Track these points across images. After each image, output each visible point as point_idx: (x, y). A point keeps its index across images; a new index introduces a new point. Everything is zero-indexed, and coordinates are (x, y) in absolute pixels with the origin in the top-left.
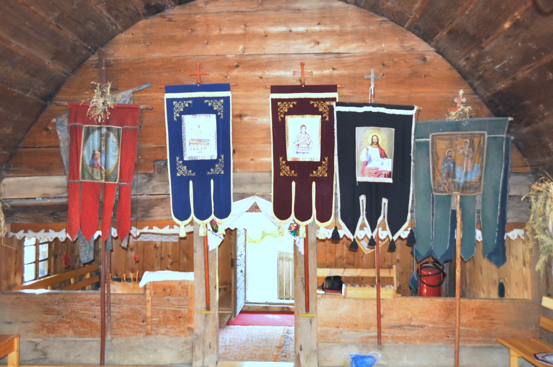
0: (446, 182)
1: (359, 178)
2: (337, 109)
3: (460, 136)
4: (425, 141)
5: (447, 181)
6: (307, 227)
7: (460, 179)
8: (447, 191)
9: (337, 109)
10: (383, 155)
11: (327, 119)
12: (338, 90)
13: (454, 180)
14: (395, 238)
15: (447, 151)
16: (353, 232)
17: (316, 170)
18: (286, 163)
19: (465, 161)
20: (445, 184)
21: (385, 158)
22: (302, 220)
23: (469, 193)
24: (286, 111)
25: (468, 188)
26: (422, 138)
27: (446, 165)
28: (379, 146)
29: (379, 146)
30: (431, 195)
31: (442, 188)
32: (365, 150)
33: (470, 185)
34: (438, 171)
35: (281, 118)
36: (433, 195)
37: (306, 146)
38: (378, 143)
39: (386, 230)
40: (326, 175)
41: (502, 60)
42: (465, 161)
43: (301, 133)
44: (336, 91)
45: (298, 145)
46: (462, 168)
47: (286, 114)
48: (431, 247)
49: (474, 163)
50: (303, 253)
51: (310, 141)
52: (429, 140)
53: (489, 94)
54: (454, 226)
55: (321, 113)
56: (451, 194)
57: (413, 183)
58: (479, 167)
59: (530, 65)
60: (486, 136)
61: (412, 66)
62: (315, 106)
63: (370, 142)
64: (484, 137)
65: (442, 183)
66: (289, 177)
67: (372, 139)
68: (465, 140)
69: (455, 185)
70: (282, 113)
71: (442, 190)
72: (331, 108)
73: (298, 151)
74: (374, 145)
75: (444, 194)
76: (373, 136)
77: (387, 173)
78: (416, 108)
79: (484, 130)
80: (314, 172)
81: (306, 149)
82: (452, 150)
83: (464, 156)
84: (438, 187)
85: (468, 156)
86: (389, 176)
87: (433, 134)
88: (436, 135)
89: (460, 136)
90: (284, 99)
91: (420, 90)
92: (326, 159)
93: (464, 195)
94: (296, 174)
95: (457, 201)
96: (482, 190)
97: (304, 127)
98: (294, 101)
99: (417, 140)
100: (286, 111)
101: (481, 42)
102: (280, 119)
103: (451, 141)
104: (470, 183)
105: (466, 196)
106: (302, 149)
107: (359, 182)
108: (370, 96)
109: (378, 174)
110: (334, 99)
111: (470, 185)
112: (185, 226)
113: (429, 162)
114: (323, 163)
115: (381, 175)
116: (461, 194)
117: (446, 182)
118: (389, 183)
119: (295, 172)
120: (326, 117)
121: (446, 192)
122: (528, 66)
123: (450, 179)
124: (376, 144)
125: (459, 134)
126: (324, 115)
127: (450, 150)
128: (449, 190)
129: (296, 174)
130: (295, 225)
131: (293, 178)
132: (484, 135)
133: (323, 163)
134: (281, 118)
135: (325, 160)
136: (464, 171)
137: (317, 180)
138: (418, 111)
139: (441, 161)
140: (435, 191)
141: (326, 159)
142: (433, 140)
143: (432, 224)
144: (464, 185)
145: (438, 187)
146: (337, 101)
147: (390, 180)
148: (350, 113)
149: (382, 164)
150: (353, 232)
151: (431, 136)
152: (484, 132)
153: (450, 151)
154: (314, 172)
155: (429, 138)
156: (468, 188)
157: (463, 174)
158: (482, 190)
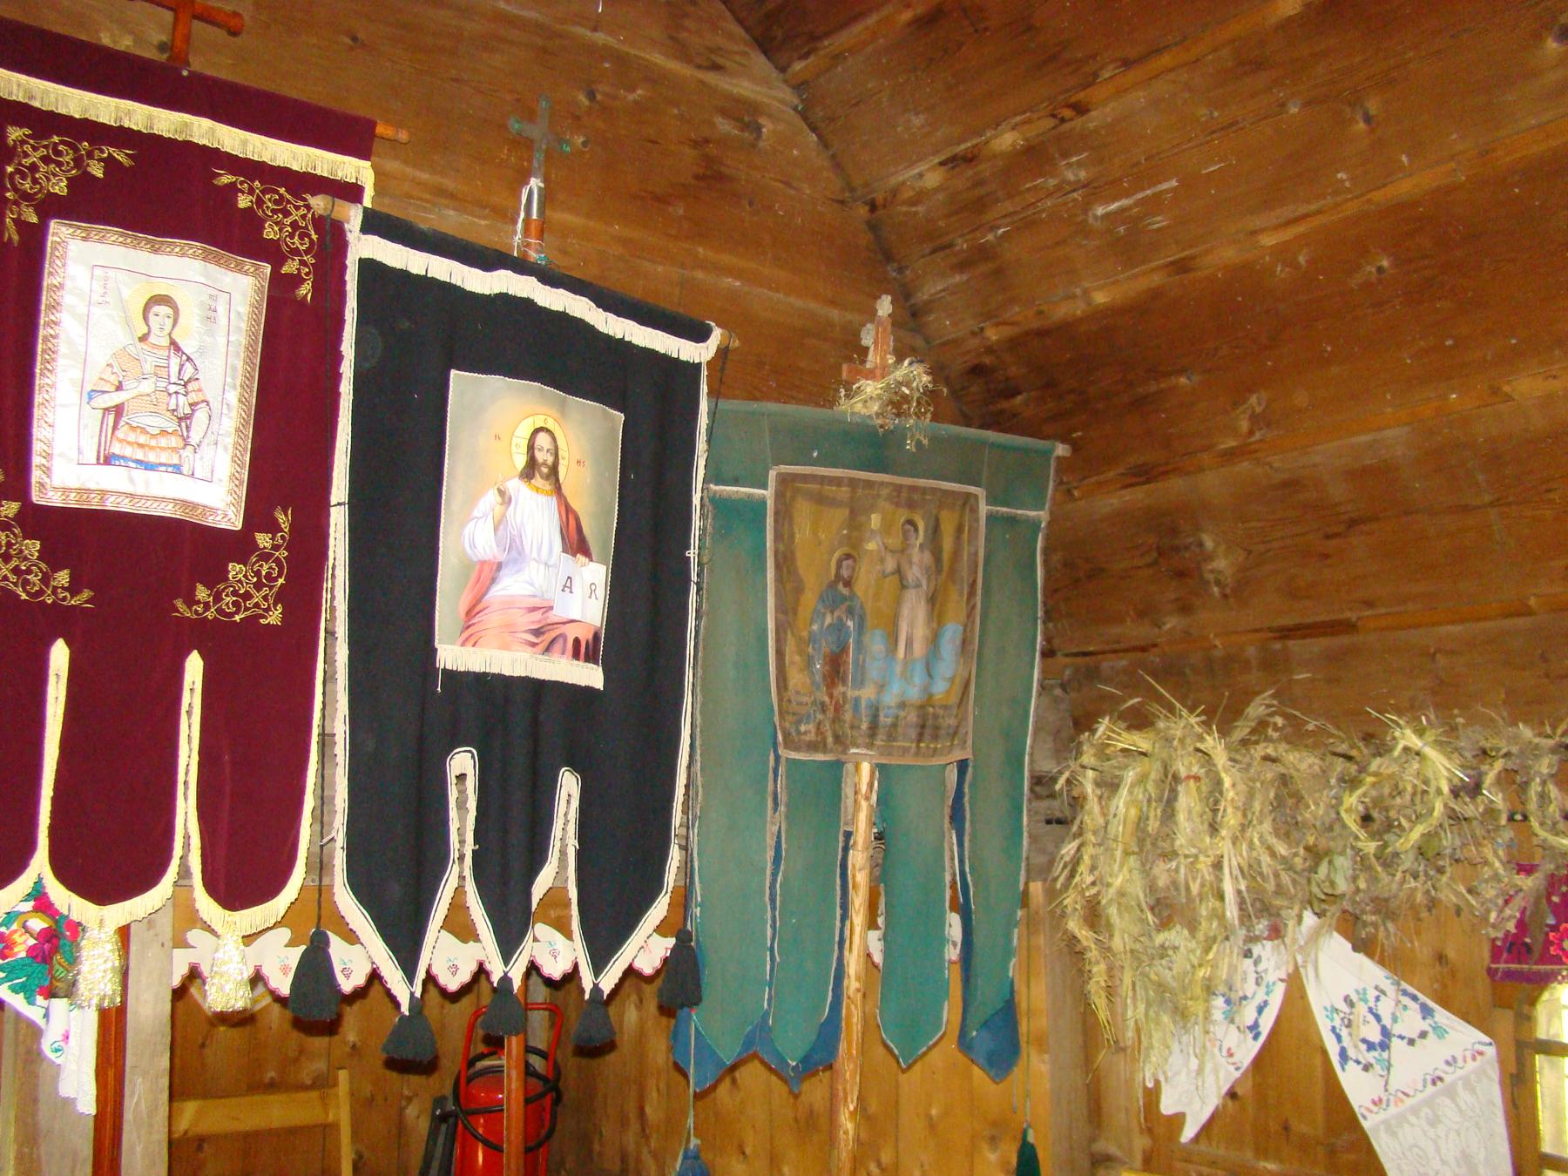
1: (451, 655)
2: (364, 247)
4: (750, 496)
5: (831, 696)
6: (124, 933)
7: (882, 687)
9: (364, 247)
10: (576, 544)
11: (305, 290)
12: (372, 158)
14: (608, 982)
15: (837, 555)
16: (406, 948)
17: (216, 578)
18: (20, 517)
20: (823, 708)
21: (581, 558)
22: (102, 891)
24: (60, 187)
26: (736, 482)
27: (828, 620)
28: (558, 489)
29: (558, 489)
32: (491, 497)
35: (20, 224)
37: (172, 426)
38: (554, 469)
39: (477, 939)
40: (274, 617)
41: (1144, 175)
43: (143, 339)
44: (362, 153)
45: (119, 410)
47: (52, 208)
48: (767, 1014)
50: (87, 1104)
51: (193, 397)
52: (768, 494)
53: (993, 335)
55: (272, 253)
59: (1303, 209)
60: (984, 508)
61: (707, 141)
62: (243, 202)
63: (521, 461)
64: (974, 510)
66: (35, 608)
67: (531, 447)
70: (26, 197)
72: (332, 239)
73: (116, 449)
74: (538, 481)
75: (820, 757)
76: (537, 431)
77: (585, 636)
78: (717, 336)
79: (977, 485)
80: (202, 593)
81: (163, 442)
86: (591, 657)
88: (796, 477)
89: (885, 492)
90: (51, 114)
91: (727, 259)
92: (283, 520)
93: (894, 761)
94: (87, 594)
97: (164, 310)
98: (119, 146)
100: (60, 187)
101: (1091, 81)
102: (12, 233)
103: (853, 513)
106: (142, 439)
107: (450, 675)
108: (520, 225)
109: (545, 636)
110: (352, 192)
112: (249, 939)
114: (263, 540)
115: (558, 646)
116: (884, 761)
117: (826, 699)
118: (589, 690)
119: (73, 578)
120: (297, 280)
121: (825, 750)
122: (1288, 211)
124: (547, 478)
125: (882, 484)
126: (290, 267)
128: (837, 738)
129: (87, 594)
130: (38, 924)
131: (60, 622)
132: (968, 501)
133: (263, 540)
134: (20, 224)
135: (273, 528)
137: (211, 637)
138: (723, 352)
139: (809, 599)
140: (789, 743)
141: (283, 520)
142: (779, 495)
143: (773, 900)
146: (367, 202)
147: (592, 676)
148: (426, 283)
149: (568, 585)
150: (406, 948)
151: (772, 474)
152: (972, 489)
154: (202, 593)
155: (764, 486)
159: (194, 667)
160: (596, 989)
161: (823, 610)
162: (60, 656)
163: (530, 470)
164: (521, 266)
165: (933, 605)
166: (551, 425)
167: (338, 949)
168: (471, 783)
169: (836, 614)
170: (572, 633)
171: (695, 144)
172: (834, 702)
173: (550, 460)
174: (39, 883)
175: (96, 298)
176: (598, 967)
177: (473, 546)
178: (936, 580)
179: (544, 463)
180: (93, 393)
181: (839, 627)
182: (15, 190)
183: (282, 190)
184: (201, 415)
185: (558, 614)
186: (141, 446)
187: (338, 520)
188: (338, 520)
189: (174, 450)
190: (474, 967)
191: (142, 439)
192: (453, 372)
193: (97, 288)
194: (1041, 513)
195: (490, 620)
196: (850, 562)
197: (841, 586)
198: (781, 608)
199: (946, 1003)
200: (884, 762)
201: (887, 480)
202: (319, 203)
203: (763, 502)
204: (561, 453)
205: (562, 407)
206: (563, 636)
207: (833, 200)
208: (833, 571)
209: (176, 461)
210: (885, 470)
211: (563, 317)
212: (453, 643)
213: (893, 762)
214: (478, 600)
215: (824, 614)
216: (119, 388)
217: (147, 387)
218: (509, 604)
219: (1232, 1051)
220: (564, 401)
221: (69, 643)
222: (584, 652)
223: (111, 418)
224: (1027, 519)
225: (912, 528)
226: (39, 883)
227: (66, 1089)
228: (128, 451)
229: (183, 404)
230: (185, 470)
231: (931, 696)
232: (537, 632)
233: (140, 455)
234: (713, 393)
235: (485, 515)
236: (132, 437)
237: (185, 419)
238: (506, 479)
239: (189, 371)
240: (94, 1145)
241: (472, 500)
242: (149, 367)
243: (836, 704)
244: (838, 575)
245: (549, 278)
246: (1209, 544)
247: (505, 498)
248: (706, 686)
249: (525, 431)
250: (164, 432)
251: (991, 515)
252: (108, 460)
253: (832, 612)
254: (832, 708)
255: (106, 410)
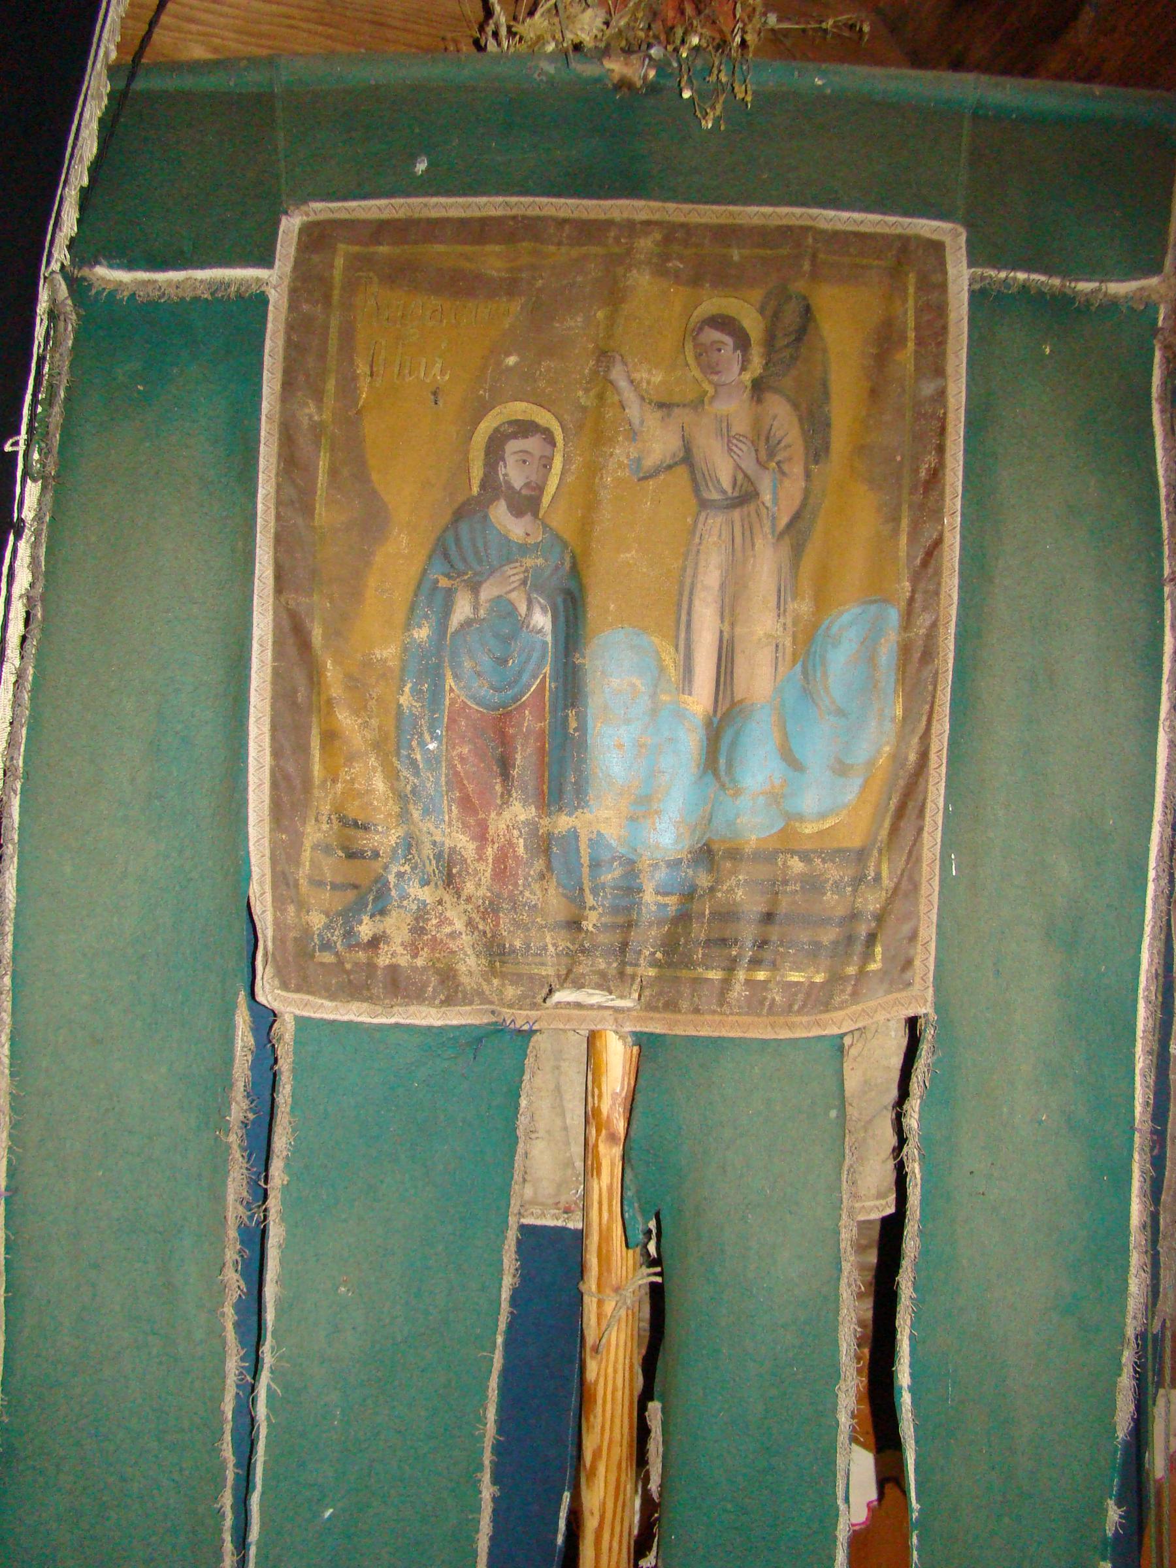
0: (465, 843)
3: (646, 244)
5: (482, 836)
8: (469, 964)
13: (564, 822)
19: (711, 576)
23: (757, 1002)
25: (748, 933)
30: (242, 1019)
31: (396, 926)
33: (774, 888)
34: (355, 684)
36: (265, 1020)
42: (711, 576)
46: (669, 657)
49: (822, 601)
54: (1153, 1224)
56: (521, 1018)
57: (1163, 411)
58: (887, 653)
65: (410, 844)
68: (713, 303)
69: (576, 899)
71: (394, 954)
82: (544, 418)
83: (704, 504)
84: (349, 916)
85: (745, 496)
87: (320, 210)
89: (646, 244)
93: (683, 1026)
95: (592, 1116)
96: (925, 960)
99: (106, 274)
104: (766, 856)
105: (717, 1043)
111: (774, 888)
113: (249, 558)
116: (656, 1027)
117: (465, 843)
123: (520, 811)
125: (632, 228)
127: (519, 409)
136: (700, 700)
144: (689, 895)
145: (349, 916)
151: (291, 225)
152: (926, 227)
153: (525, 428)
155: (266, 260)
156: (748, 933)
157: (690, 742)
158: (925, 960)
161: (444, 582)
165: (798, 551)
169: (487, 592)
172: (490, 852)
178: (808, 475)
194: (1154, 281)
197: (500, 513)
200: (657, 1028)
201: (643, 216)
203: (261, 301)
208: (477, 472)
210: (633, 188)
213: (679, 1031)
215: (449, 594)
225: (728, 340)
231: (793, 818)
240: (663, 1321)
243: (501, 859)
244: (491, 486)
251: (983, 292)
253: (475, 588)
254: (486, 871)
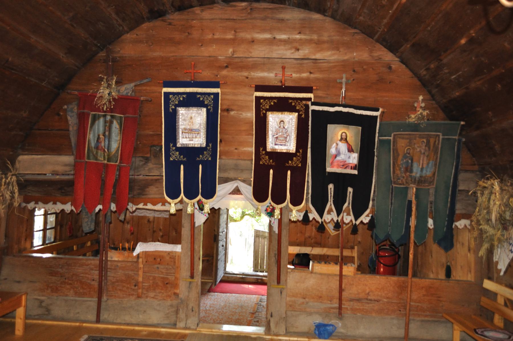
1: (329, 169)
4: (388, 139)
5: (405, 175)
6: (281, 209)
7: (416, 173)
10: (350, 150)
11: (303, 116)
12: (314, 92)
14: (358, 222)
15: (406, 148)
17: (292, 160)
20: (404, 177)
22: (278, 204)
24: (268, 107)
26: (385, 136)
27: (404, 161)
35: (263, 113)
39: (350, 215)
43: (280, 127)
45: (277, 138)
50: (277, 232)
51: (287, 134)
52: (391, 138)
53: (445, 101)
60: (441, 137)
62: (293, 104)
64: (439, 137)
67: (341, 136)
72: (307, 107)
73: (277, 143)
74: (343, 141)
75: (402, 186)
76: (342, 133)
81: (283, 141)
94: (274, 163)
100: (268, 107)
106: (280, 141)
109: (345, 165)
114: (298, 154)
115: (348, 167)
117: (405, 176)
118: (355, 175)
119: (273, 161)
121: (403, 184)
124: (344, 140)
126: (301, 113)
129: (274, 163)
132: (439, 136)
134: (263, 113)
138: (383, 113)
139: (400, 157)
142: (394, 138)
147: (356, 172)
148: (323, 111)
149: (349, 157)
151: (392, 135)
152: (439, 133)
159: (289, 172)
160: (355, 224)
162: (271, 171)
163: (341, 139)
164: (339, 105)
166: (345, 131)
167: (310, 215)
168: (332, 189)
170: (350, 165)
171: (377, 74)
173: (345, 137)
174: (182, 198)
175: (273, 122)
176: (356, 220)
177: (332, 152)
179: (344, 138)
180: (273, 136)
181: (407, 162)
182: (262, 109)
183: (299, 101)
184: (288, 137)
185: (347, 162)
186: (281, 142)
187: (309, 150)
188: (309, 150)
189: (285, 142)
190: (331, 219)
191: (280, 141)
192: (328, 125)
193: (273, 121)
195: (335, 164)
196: (409, 150)
198: (394, 159)
199: (427, 234)
202: (304, 102)
204: (347, 136)
205: (348, 128)
206: (349, 166)
207: (410, 77)
209: (285, 144)
211: (348, 113)
212: (329, 167)
214: (333, 161)
216: (277, 134)
217: (280, 134)
218: (338, 161)
219: (510, 252)
220: (348, 127)
221: (273, 169)
222: (354, 168)
223: (276, 139)
224: (453, 139)
226: (182, 198)
227: (274, 230)
228: (278, 143)
229: (285, 136)
230: (286, 145)
232: (343, 166)
233: (280, 144)
234: (253, 152)
235: (334, 147)
236: (279, 141)
237: (286, 138)
238: (337, 141)
239: (286, 131)
241: (331, 145)
242: (280, 131)
245: (345, 106)
246: (494, 142)
247: (337, 144)
248: (377, 174)
249: (340, 133)
250: (283, 140)
252: (276, 145)
255: (275, 138)
